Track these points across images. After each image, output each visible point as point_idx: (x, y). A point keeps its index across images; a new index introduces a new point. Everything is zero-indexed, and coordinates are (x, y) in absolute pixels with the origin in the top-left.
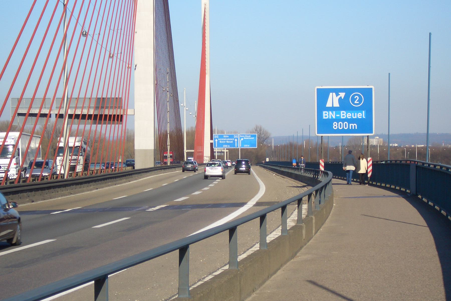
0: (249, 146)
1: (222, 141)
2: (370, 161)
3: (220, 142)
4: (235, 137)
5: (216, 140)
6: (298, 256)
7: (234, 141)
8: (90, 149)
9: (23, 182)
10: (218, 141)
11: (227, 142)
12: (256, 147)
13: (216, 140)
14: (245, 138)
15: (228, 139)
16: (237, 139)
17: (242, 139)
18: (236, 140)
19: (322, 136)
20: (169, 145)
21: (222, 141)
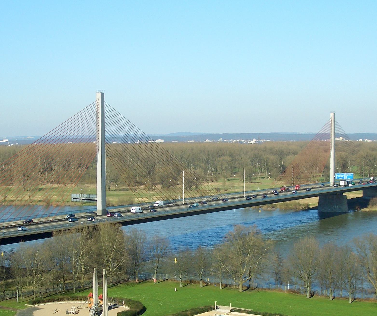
0: (350, 178)
1: (339, 176)
2: (56, 194)
3: (338, 177)
4: (344, 174)
5: (336, 176)
6: (353, 196)
7: (344, 176)
8: (231, 158)
9: (257, 178)
10: (337, 176)
11: (341, 177)
12: (353, 179)
13: (336, 176)
14: (348, 175)
15: (341, 175)
16: (345, 175)
17: (347, 176)
18: (344, 176)
19: (97, 201)
20: (43, 220)
21: (339, 176)
